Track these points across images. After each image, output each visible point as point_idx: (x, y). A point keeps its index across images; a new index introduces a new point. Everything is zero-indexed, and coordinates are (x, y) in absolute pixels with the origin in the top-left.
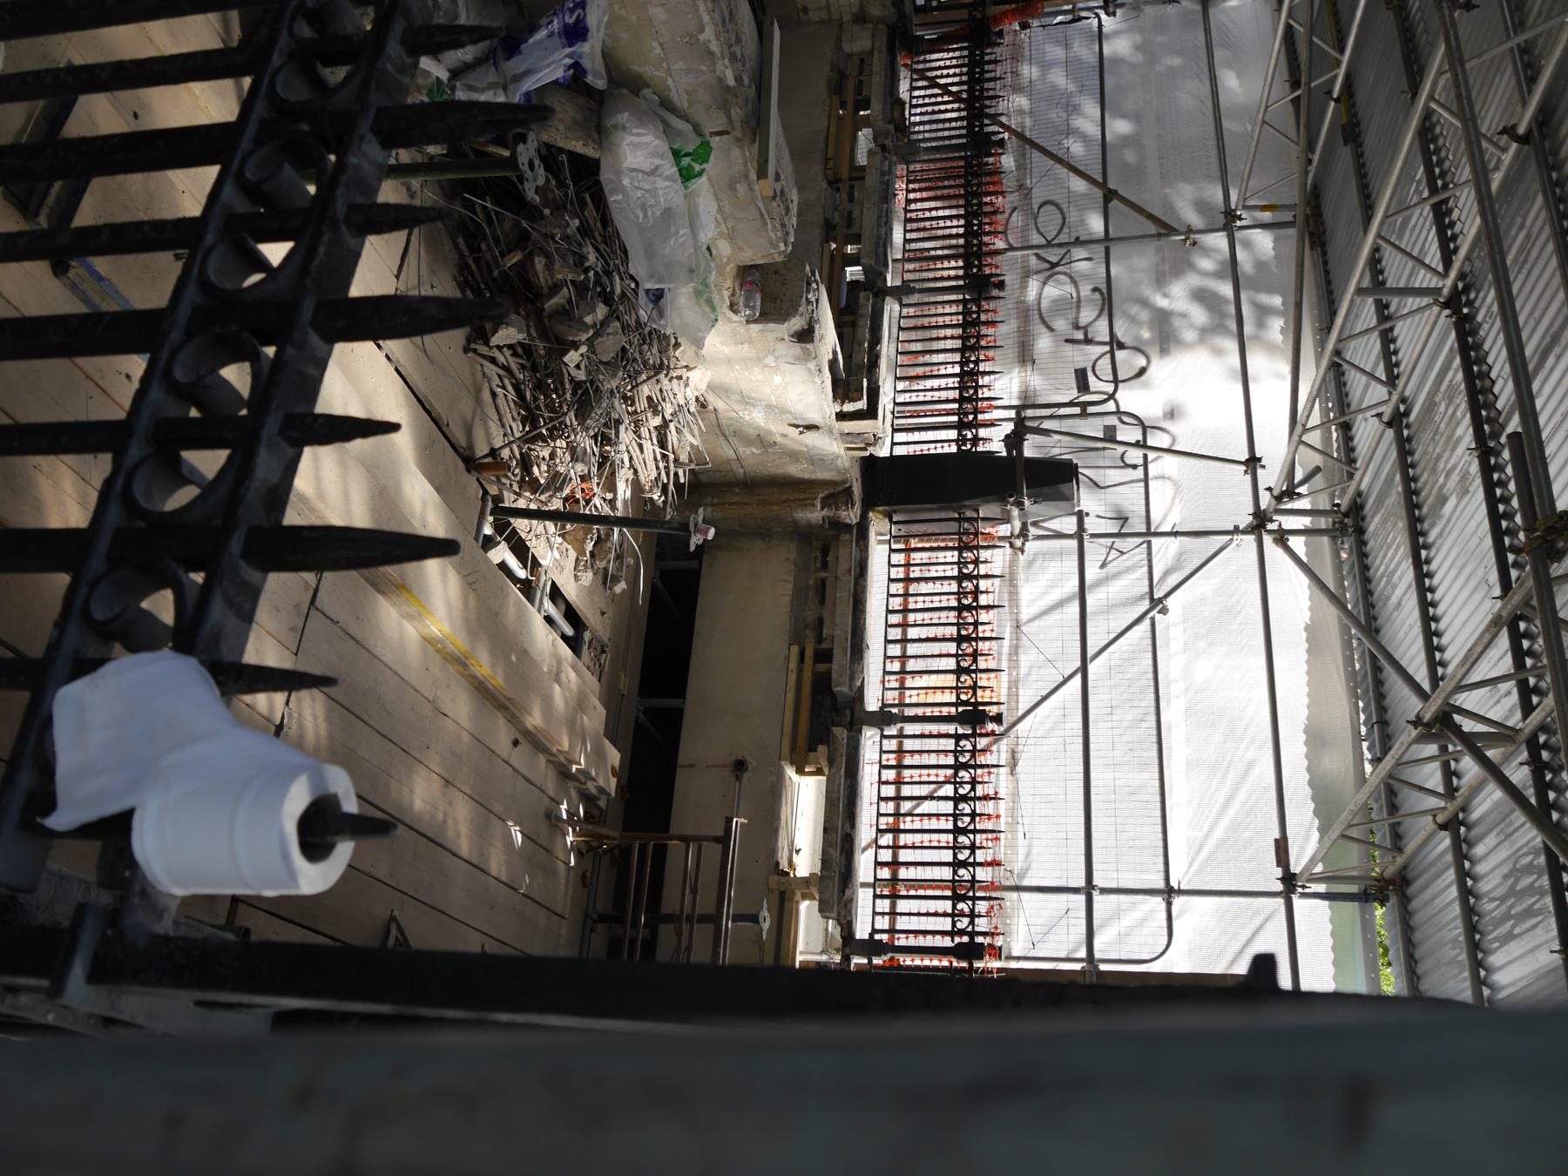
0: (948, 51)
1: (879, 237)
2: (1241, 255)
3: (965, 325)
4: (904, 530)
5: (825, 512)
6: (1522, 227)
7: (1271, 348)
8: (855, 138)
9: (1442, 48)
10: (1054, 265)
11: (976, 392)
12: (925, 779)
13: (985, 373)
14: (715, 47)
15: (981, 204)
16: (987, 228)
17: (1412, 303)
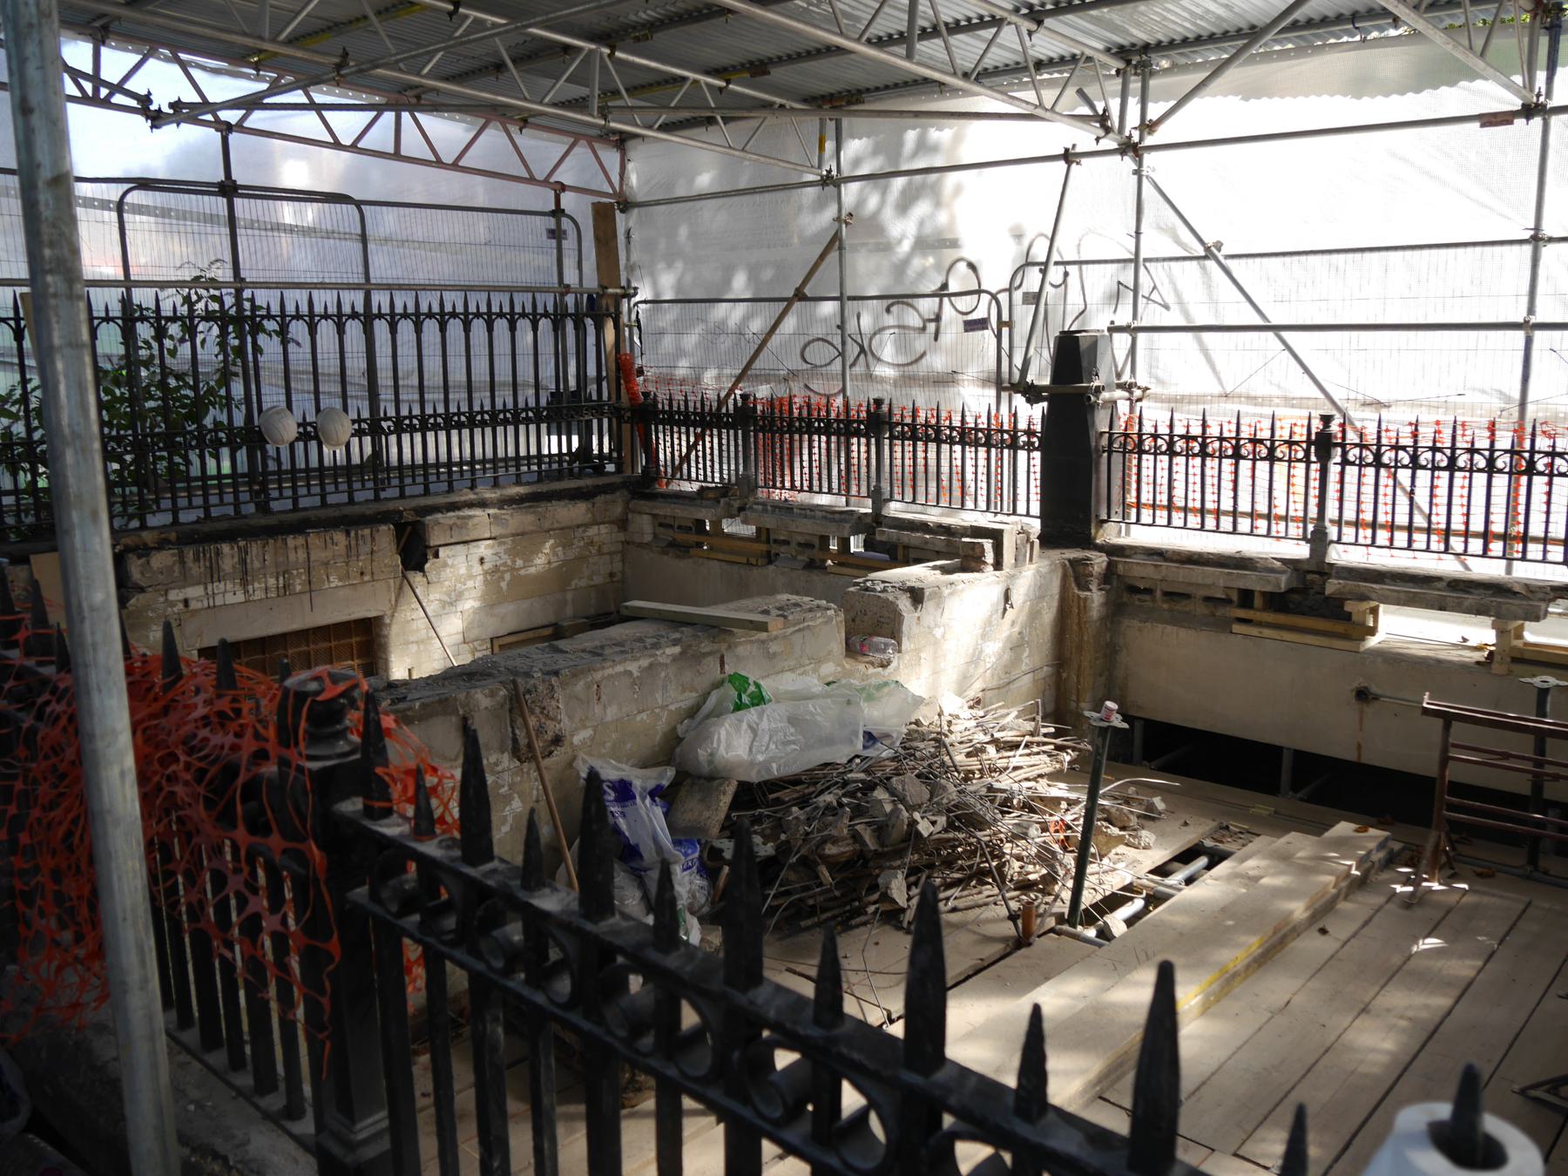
1: (825, 518)
3: (914, 438)
4: (1117, 508)
5: (1094, 587)
12: (1389, 499)
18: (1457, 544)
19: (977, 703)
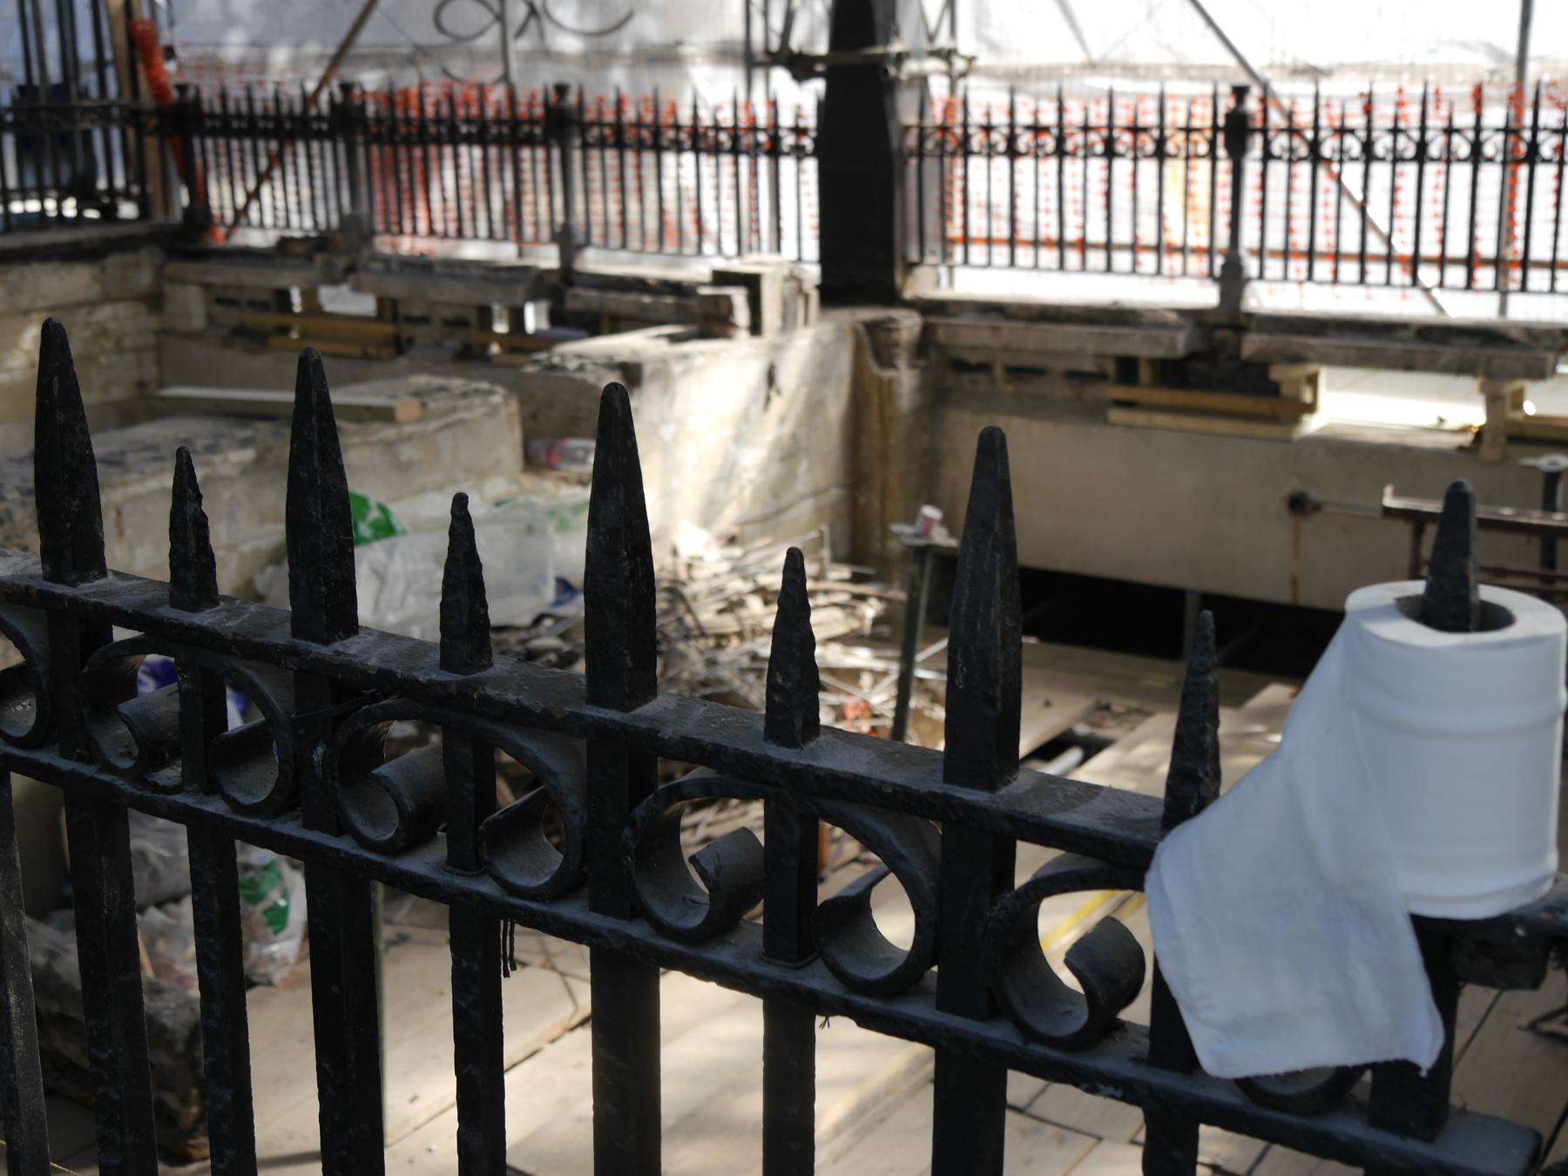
1: (484, 278)
3: (620, 145)
4: (933, 245)
5: (902, 363)
12: (1332, 211)
13: (695, 117)
18: (1428, 275)
19: (732, 540)
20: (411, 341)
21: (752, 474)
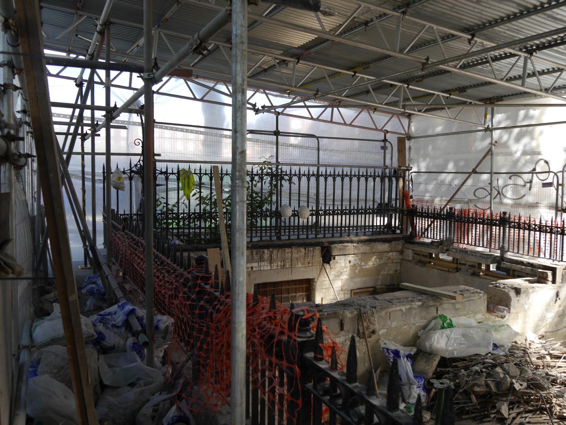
0: (416, 224)
1: (480, 256)
2: (502, 125)
6: (505, 33)
7: (542, 114)
8: (442, 260)
9: (441, 66)
10: (499, 193)
11: (548, 227)
13: (540, 222)
14: (408, 307)
15: (472, 218)
16: (482, 216)
17: (529, 65)
20: (460, 269)
21: (550, 320)
